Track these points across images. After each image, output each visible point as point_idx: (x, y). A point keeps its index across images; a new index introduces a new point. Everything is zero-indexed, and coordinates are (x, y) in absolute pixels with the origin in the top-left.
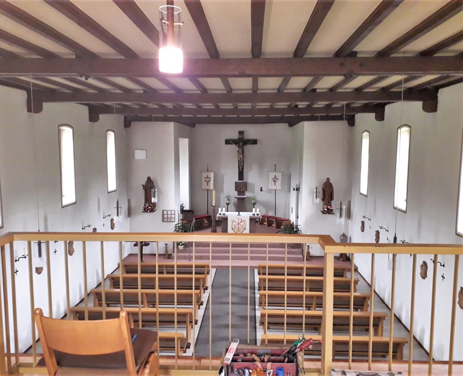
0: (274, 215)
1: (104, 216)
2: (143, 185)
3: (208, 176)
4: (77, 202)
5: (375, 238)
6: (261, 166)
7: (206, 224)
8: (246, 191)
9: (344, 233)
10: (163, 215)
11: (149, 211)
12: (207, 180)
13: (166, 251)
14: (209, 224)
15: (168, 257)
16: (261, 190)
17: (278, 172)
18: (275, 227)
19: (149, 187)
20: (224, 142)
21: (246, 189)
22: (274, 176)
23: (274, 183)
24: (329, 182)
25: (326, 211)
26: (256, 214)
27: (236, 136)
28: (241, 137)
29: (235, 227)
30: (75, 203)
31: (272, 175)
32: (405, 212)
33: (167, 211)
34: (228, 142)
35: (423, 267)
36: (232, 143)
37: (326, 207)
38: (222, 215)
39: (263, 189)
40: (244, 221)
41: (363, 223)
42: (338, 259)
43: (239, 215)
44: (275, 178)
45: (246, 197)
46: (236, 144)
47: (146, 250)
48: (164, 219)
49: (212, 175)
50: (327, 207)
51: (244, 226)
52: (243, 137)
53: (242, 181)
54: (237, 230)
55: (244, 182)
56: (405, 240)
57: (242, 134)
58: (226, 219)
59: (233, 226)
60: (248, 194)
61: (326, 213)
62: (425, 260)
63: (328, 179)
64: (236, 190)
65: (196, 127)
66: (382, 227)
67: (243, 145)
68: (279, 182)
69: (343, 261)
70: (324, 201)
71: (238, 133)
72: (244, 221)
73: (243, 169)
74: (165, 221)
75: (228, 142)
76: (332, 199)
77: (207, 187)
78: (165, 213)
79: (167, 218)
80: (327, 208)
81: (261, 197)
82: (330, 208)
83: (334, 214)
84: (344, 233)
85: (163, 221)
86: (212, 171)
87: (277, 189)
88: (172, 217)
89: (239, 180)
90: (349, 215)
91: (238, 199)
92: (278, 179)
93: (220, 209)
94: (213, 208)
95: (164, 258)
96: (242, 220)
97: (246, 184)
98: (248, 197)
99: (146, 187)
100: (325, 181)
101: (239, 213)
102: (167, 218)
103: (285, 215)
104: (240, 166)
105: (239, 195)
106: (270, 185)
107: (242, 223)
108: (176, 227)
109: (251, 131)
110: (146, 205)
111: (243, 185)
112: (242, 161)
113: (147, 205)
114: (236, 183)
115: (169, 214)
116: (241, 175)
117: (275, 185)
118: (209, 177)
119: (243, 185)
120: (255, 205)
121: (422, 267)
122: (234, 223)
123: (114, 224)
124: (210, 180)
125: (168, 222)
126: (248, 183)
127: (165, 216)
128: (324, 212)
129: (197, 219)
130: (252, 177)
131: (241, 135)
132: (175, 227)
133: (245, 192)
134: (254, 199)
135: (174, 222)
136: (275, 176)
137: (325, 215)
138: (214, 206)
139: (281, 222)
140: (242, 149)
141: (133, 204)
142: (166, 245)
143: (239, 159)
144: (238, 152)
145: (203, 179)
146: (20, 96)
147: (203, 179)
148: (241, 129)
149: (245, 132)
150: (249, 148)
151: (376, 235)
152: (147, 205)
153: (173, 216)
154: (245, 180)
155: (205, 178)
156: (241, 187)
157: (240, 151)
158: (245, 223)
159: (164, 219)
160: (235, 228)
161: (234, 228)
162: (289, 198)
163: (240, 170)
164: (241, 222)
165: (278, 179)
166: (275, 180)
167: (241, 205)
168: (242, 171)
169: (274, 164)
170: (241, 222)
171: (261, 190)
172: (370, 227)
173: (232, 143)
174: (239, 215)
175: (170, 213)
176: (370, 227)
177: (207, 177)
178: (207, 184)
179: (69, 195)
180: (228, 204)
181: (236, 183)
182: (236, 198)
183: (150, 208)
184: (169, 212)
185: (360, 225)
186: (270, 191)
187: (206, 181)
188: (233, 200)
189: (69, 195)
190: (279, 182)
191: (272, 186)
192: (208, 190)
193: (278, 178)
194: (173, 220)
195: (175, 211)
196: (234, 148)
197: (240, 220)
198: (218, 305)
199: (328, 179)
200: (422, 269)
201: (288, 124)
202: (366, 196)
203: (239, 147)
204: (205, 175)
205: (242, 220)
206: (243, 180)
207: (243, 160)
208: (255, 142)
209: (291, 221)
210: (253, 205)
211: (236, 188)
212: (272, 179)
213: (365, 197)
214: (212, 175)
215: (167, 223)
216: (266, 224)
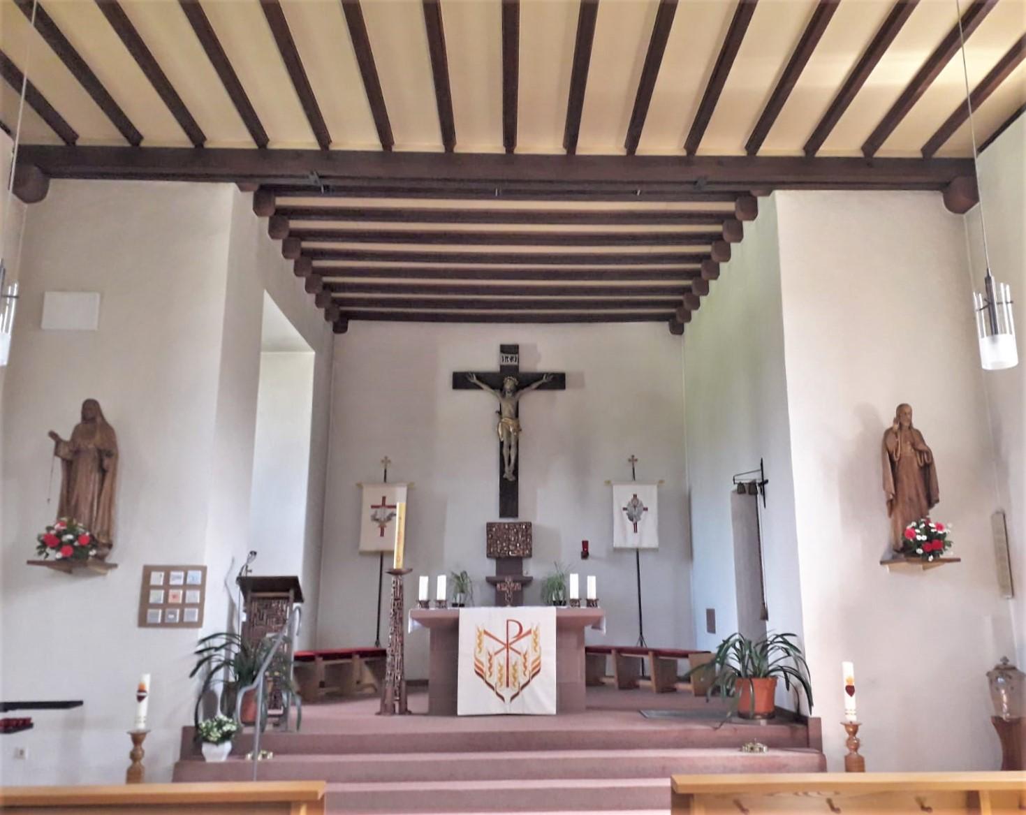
3: (384, 498)
8: (530, 556)
9: (1005, 660)
12: (381, 514)
16: (585, 555)
17: (645, 482)
19: (91, 453)
20: (448, 380)
23: (630, 524)
27: (491, 362)
28: (509, 363)
29: (490, 660)
34: (461, 381)
44: (635, 507)
48: (150, 611)
51: (531, 659)
52: (514, 363)
53: (511, 520)
54: (500, 679)
55: (520, 524)
59: (484, 659)
63: (903, 412)
68: (649, 522)
70: (898, 510)
71: (498, 349)
73: (516, 472)
74: (150, 619)
75: (461, 381)
76: (934, 499)
77: (379, 545)
78: (157, 578)
79: (166, 605)
85: (143, 622)
86: (398, 482)
89: (502, 515)
92: (646, 509)
93: (424, 582)
97: (526, 530)
104: (506, 462)
107: (524, 644)
109: (544, 346)
111: (517, 533)
112: (513, 458)
115: (172, 582)
117: (636, 530)
118: (387, 503)
119: (517, 533)
125: (164, 624)
127: (156, 596)
130: (545, 505)
131: (510, 356)
132: (200, 652)
133: (525, 562)
136: (635, 496)
140: (514, 403)
142: (137, 738)
144: (500, 413)
145: (367, 513)
147: (367, 513)
148: (509, 341)
150: (533, 401)
154: (523, 517)
155: (373, 507)
157: (508, 409)
159: (150, 611)
160: (490, 668)
161: (485, 669)
163: (505, 476)
164: (520, 636)
165: (646, 509)
170: (520, 636)
171: (585, 555)
177: (380, 503)
178: (379, 530)
183: (70, 537)
184: (173, 574)
187: (375, 519)
190: (649, 522)
191: (625, 536)
193: (645, 506)
195: (204, 569)
196: (483, 401)
197: (514, 630)
199: (903, 412)
204: (372, 496)
205: (525, 630)
206: (516, 515)
208: (557, 381)
211: (489, 546)
212: (625, 509)
215: (161, 631)
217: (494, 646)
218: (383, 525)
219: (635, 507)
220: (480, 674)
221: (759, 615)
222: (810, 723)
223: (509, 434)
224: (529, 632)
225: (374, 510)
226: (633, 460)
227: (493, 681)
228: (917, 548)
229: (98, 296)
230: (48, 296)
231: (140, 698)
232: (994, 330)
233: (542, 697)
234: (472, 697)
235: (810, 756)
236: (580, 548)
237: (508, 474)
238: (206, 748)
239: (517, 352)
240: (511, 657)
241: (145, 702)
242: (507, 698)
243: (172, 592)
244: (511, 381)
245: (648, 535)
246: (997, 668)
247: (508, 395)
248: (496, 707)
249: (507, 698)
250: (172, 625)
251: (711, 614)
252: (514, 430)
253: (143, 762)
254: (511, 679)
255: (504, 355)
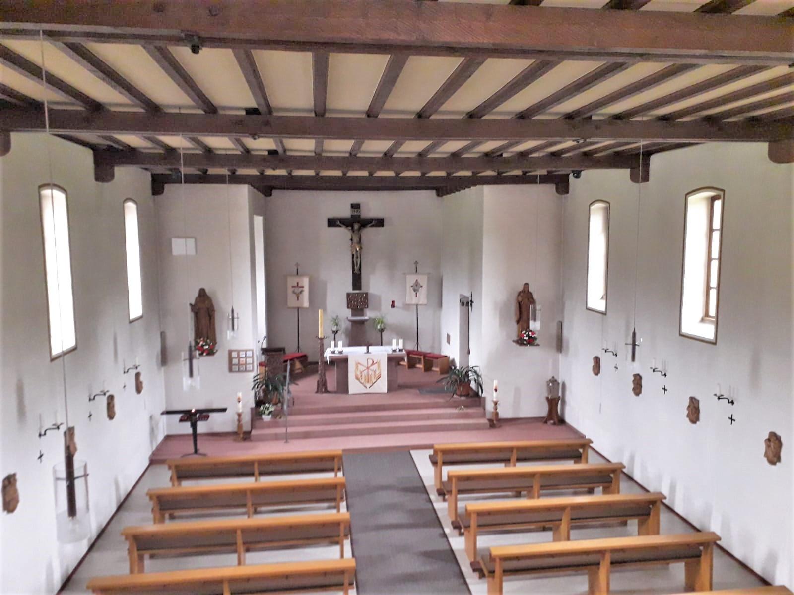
0: (415, 347)
1: (124, 369)
2: (191, 305)
3: (298, 283)
4: (79, 347)
5: (632, 386)
6: (392, 264)
7: (299, 369)
9: (553, 377)
10: (230, 359)
11: (205, 354)
12: (298, 290)
13: (240, 426)
14: (303, 369)
15: (243, 438)
16: (393, 306)
18: (423, 370)
20: (326, 223)
21: (366, 305)
22: (415, 280)
23: (414, 293)
24: (528, 291)
25: (525, 340)
26: (398, 350)
27: (346, 212)
28: (356, 214)
29: (361, 373)
30: (74, 349)
31: (411, 280)
32: (715, 343)
33: (238, 352)
34: (332, 223)
35: (772, 444)
36: (340, 224)
37: (525, 333)
38: (337, 355)
39: (396, 304)
40: (378, 363)
41: (597, 360)
42: (546, 422)
43: (368, 352)
45: (366, 318)
46: (347, 226)
47: (202, 427)
49: (305, 282)
50: (527, 333)
51: (377, 372)
54: (365, 380)
55: (363, 293)
56: (722, 393)
57: (357, 208)
58: (345, 361)
60: (369, 314)
61: (526, 345)
62: (773, 430)
63: (526, 284)
64: (348, 307)
65: (273, 195)
66: (656, 369)
67: (360, 229)
69: (554, 424)
70: (520, 323)
71: (349, 206)
72: (378, 363)
73: (360, 270)
74: (233, 370)
75: (332, 223)
78: (234, 355)
79: (239, 364)
80: (528, 336)
81: (392, 317)
82: (533, 336)
83: (538, 345)
84: (553, 377)
85: (231, 370)
86: (303, 275)
87: (421, 303)
88: (247, 362)
89: (354, 289)
90: (560, 345)
91: (354, 323)
92: (422, 287)
94: (319, 341)
95: (235, 440)
96: (373, 362)
97: (365, 298)
98: (370, 318)
99: (197, 308)
100: (521, 288)
101: (368, 348)
102: (239, 364)
103: (432, 347)
105: (353, 315)
106: (408, 298)
107: (375, 367)
108: (257, 380)
110: (199, 343)
112: (359, 256)
113: (201, 343)
114: (348, 295)
116: (357, 280)
117: (416, 296)
119: (361, 297)
120: (383, 333)
121: (768, 443)
122: (361, 368)
123: (141, 383)
124: (301, 292)
125: (239, 371)
126: (369, 296)
127: (235, 361)
128: (520, 342)
129: (287, 365)
130: (376, 284)
131: (356, 210)
132: (255, 381)
133: (365, 310)
134: (382, 322)
135: (253, 371)
136: (417, 280)
137: (523, 347)
138: (321, 339)
139: (430, 360)
141: (171, 341)
143: (354, 253)
144: (352, 240)
146: (87, 156)
147: (290, 290)
148: (355, 201)
149: (361, 206)
150: (369, 233)
151: (636, 382)
152: (201, 343)
153: (249, 361)
155: (293, 287)
156: (358, 301)
157: (356, 239)
158: (379, 366)
160: (361, 376)
161: (359, 377)
162: (439, 318)
165: (422, 287)
166: (416, 287)
167: (359, 334)
168: (358, 272)
169: (415, 261)
171: (393, 306)
172: (616, 368)
173: (340, 224)
174: (368, 352)
175: (244, 356)
176: (616, 368)
177: (296, 285)
178: (296, 299)
179: (63, 333)
180: (335, 333)
181: (348, 295)
182: (350, 321)
183: (207, 347)
185: (592, 363)
186: (407, 307)
187: (294, 292)
188: (345, 325)
189: (63, 333)
190: (423, 292)
192: (298, 309)
194: (249, 367)
196: (343, 233)
197: (370, 362)
198: (373, 533)
199: (526, 284)
200: (768, 446)
201: (434, 192)
202: (604, 314)
203: (353, 230)
204: (292, 281)
206: (360, 288)
207: (360, 255)
208: (380, 223)
209: (449, 357)
210: (380, 333)
212: (412, 286)
213: (600, 315)
214: (305, 282)
215: (238, 374)
216: (405, 366)
217: (361, 368)
218: (298, 296)
219: (417, 285)
220: (357, 378)
221: (467, 351)
222: (482, 399)
223: (357, 251)
224: (376, 363)
225: (293, 288)
226: (416, 263)
227: (363, 381)
228: (526, 340)
229: (193, 240)
230: (173, 240)
231: (239, 402)
232: (535, 320)
233: (382, 386)
234: (354, 386)
235: (480, 410)
236: (391, 303)
237: (356, 271)
238: (263, 416)
239: (359, 208)
240: (368, 367)
241: (241, 403)
242: (368, 387)
243: (241, 359)
244: (357, 223)
245: (422, 298)
246: (550, 380)
247: (356, 232)
248: (363, 390)
249: (368, 387)
250: (242, 371)
251: (448, 337)
252: (359, 250)
253: (242, 423)
254: (369, 380)
255: (354, 210)
